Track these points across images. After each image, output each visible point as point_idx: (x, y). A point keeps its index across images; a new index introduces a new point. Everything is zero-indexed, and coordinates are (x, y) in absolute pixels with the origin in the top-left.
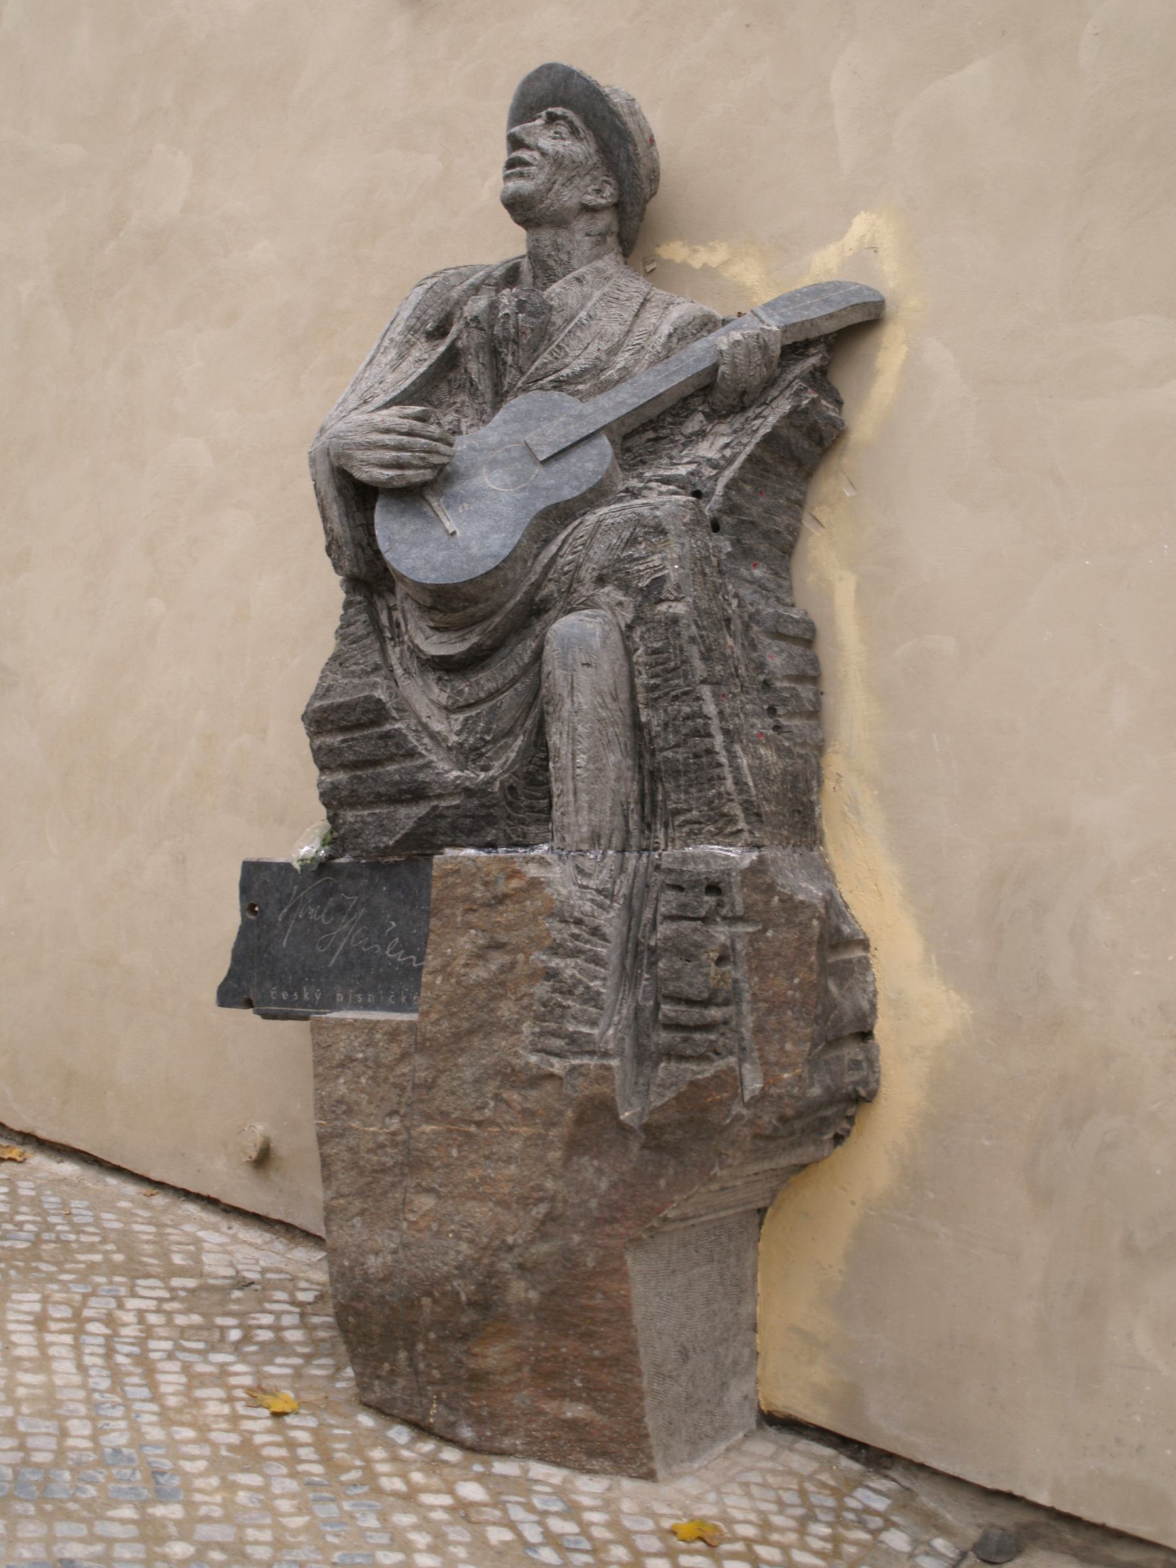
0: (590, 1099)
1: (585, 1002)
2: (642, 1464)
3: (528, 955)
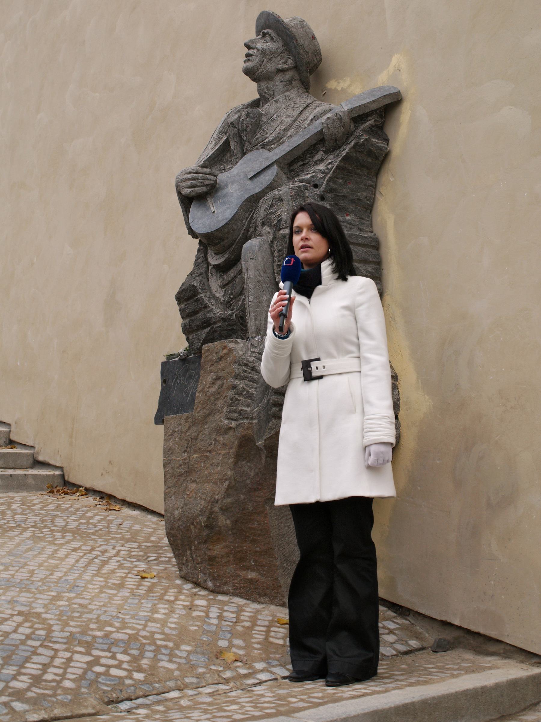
0: (244, 436)
1: (247, 397)
2: (280, 600)
3: (227, 380)
